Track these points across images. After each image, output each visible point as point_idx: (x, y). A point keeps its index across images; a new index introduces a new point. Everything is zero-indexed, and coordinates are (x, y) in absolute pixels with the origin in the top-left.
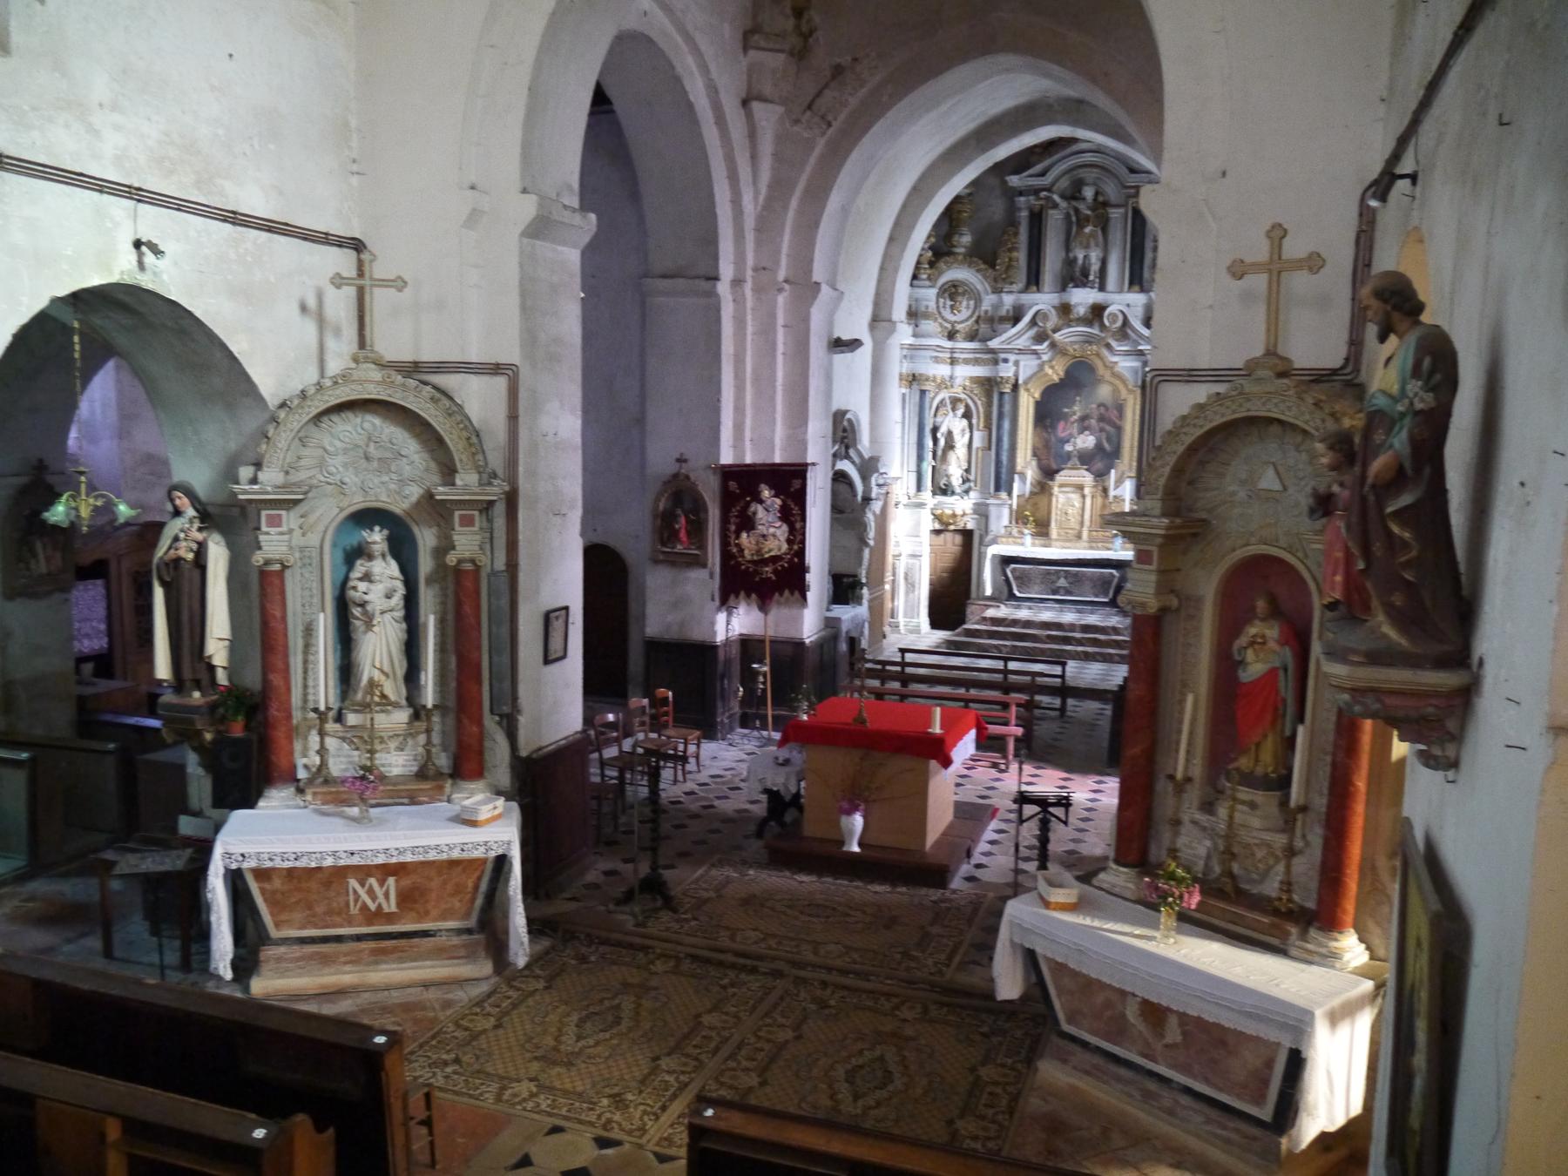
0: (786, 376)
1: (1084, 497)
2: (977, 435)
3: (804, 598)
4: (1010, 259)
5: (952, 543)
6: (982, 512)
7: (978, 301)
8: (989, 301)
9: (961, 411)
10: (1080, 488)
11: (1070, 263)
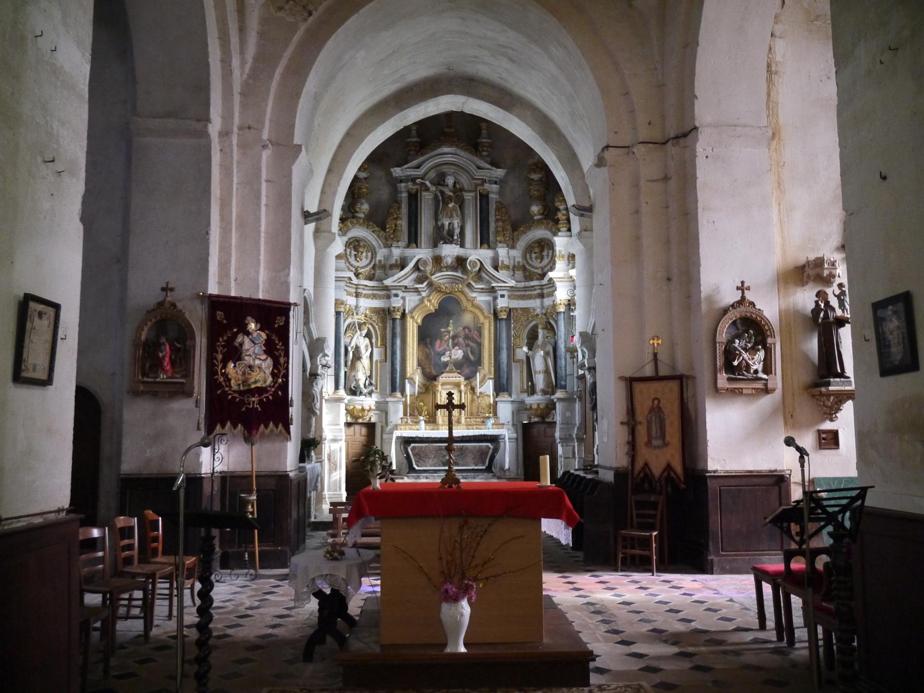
0: (267, 225)
1: (460, 392)
2: (376, 351)
3: (288, 431)
5: (360, 433)
6: (382, 408)
7: (374, 254)
8: (381, 253)
9: (364, 332)
11: (438, 229)
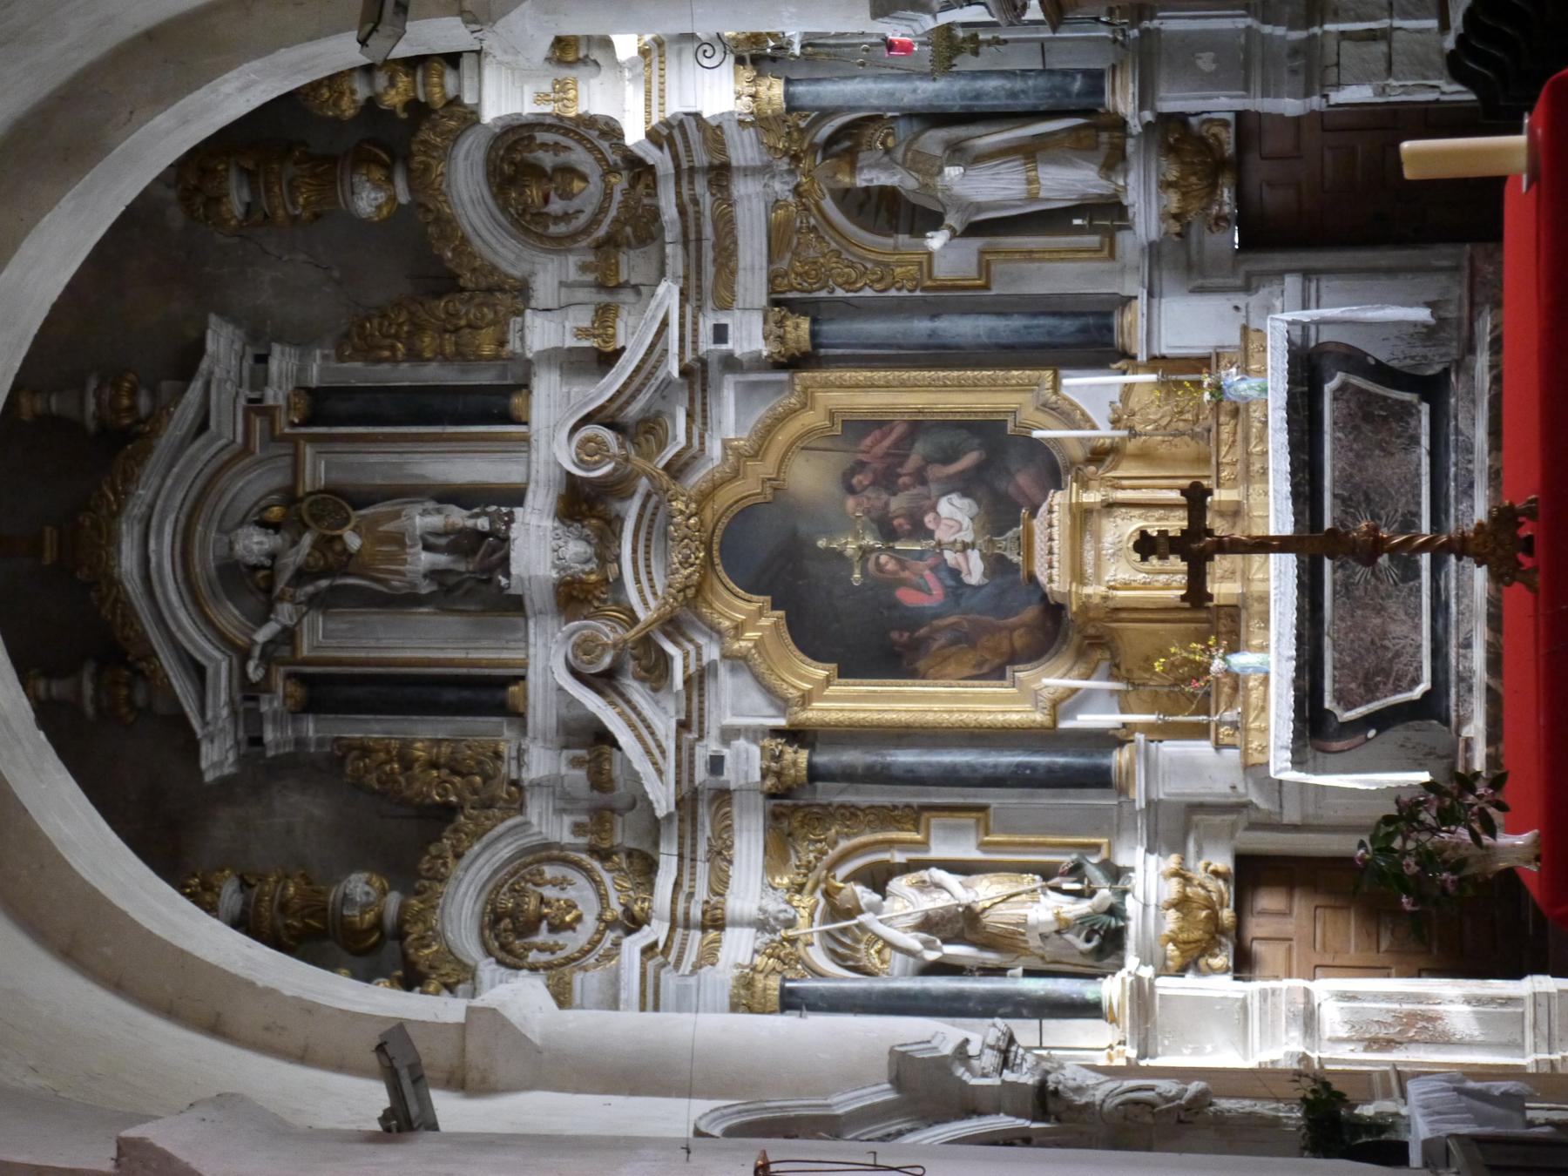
1: (1110, 506)
4: (434, 765)
7: (547, 853)
9: (865, 895)
10: (1083, 518)
